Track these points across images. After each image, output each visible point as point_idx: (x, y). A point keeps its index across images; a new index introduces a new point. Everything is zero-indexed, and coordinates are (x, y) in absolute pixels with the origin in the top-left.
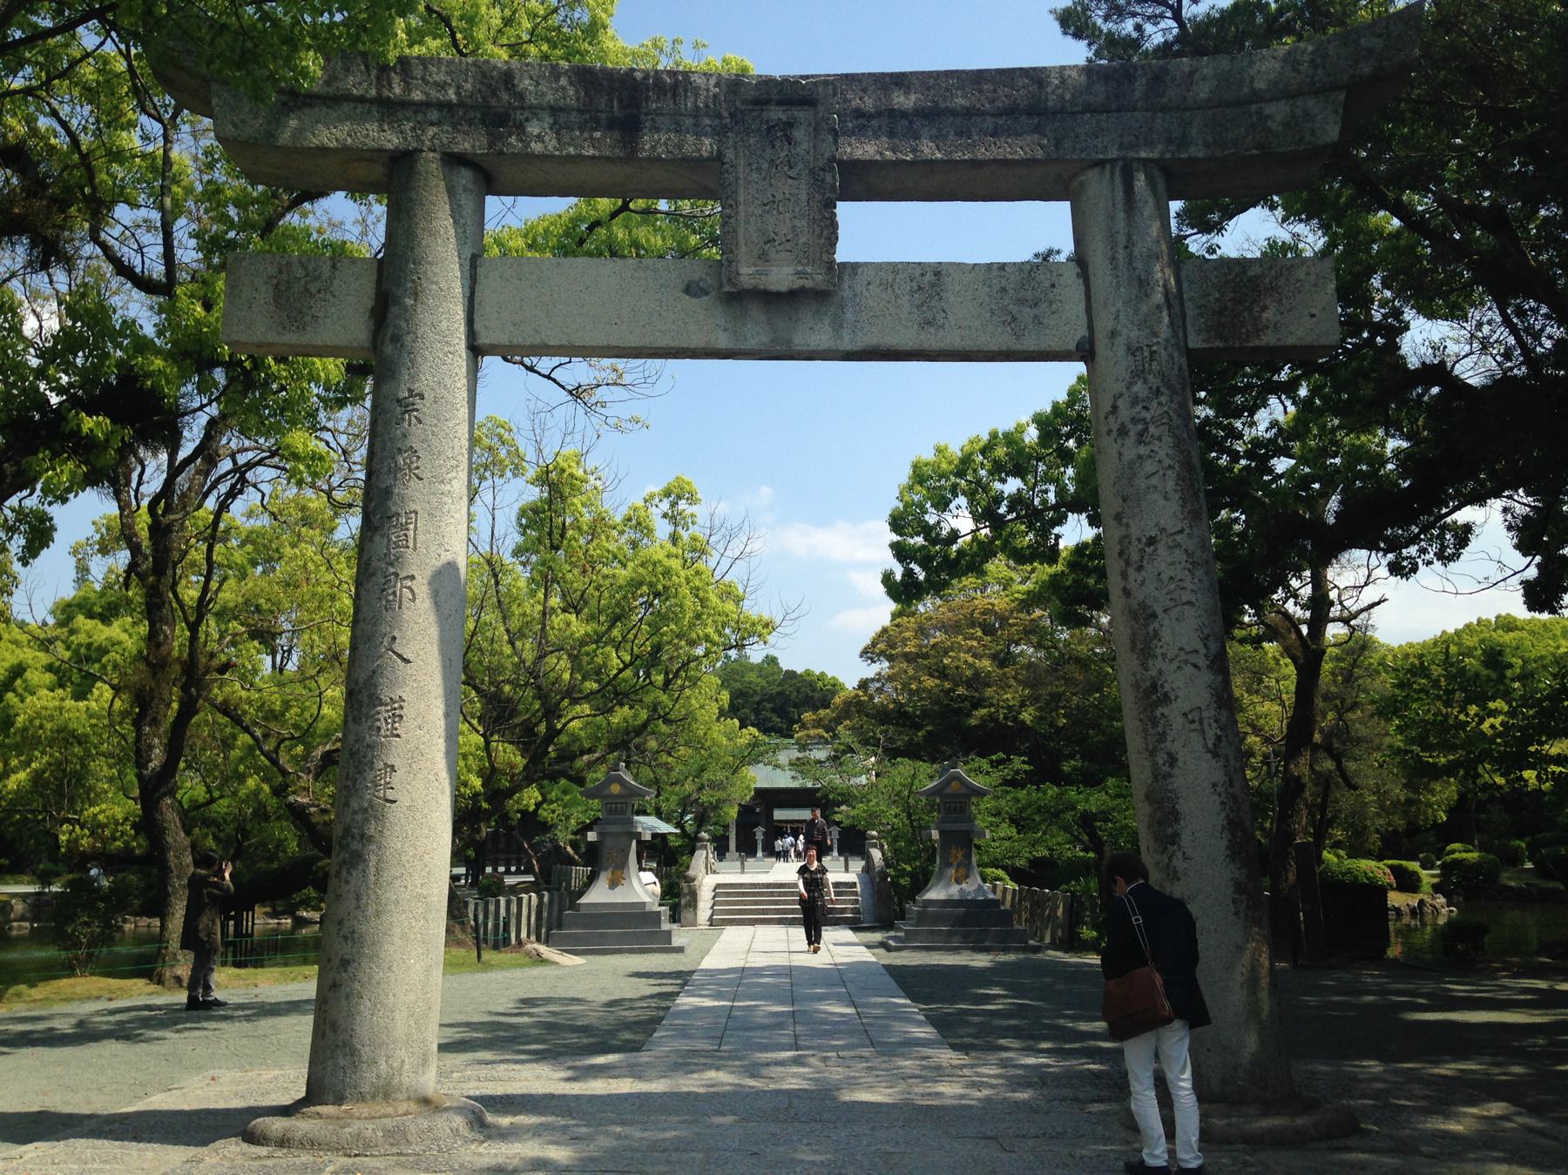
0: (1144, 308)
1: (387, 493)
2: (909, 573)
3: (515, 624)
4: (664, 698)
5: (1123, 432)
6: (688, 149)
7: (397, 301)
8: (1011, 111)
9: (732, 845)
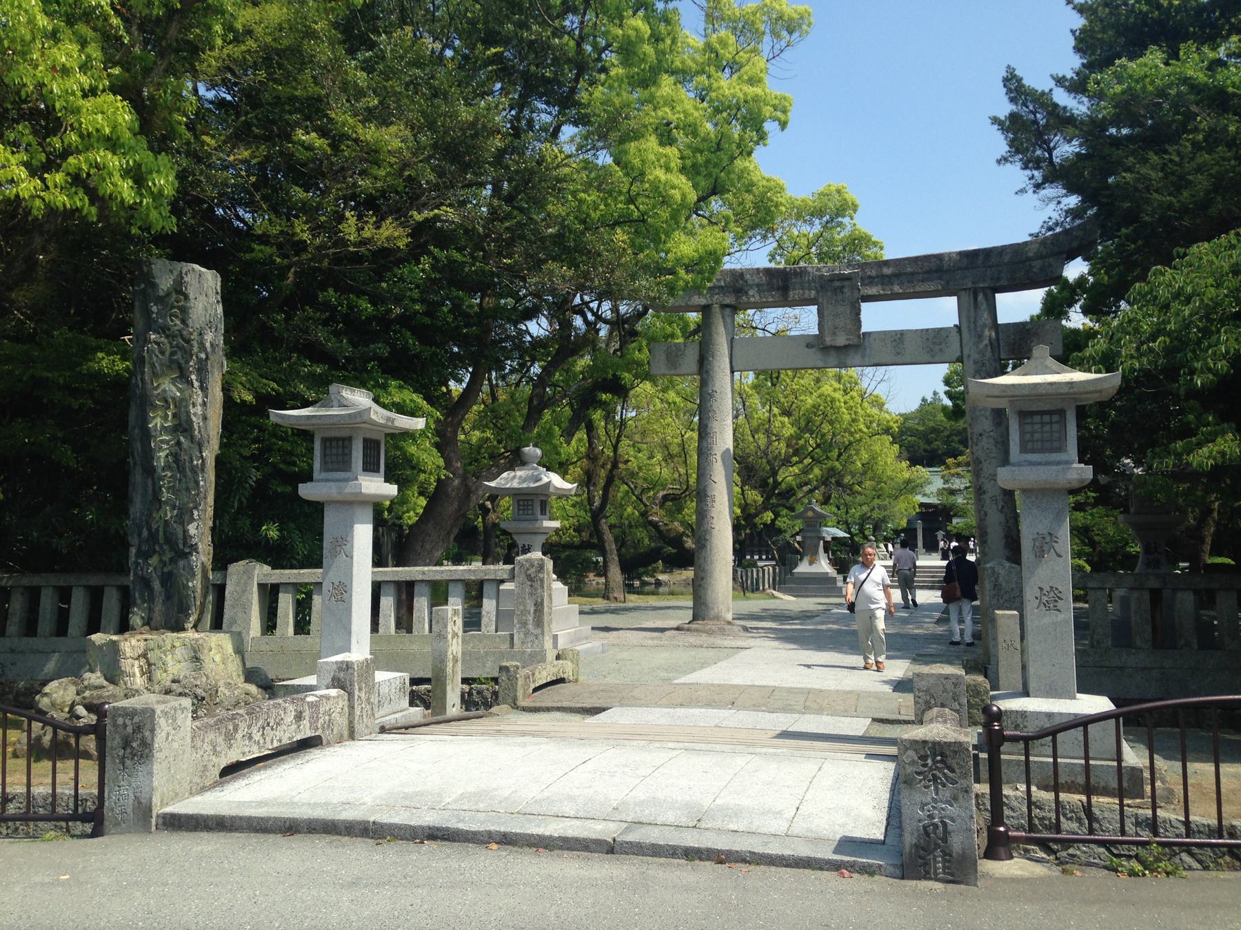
0: (981, 346)
1: (706, 426)
3: (755, 423)
4: (837, 464)
6: (806, 296)
8: (929, 272)
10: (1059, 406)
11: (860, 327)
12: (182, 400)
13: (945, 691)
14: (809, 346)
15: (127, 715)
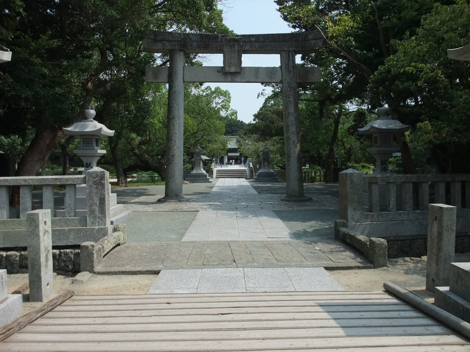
9: (218, 162)
14: (218, 72)
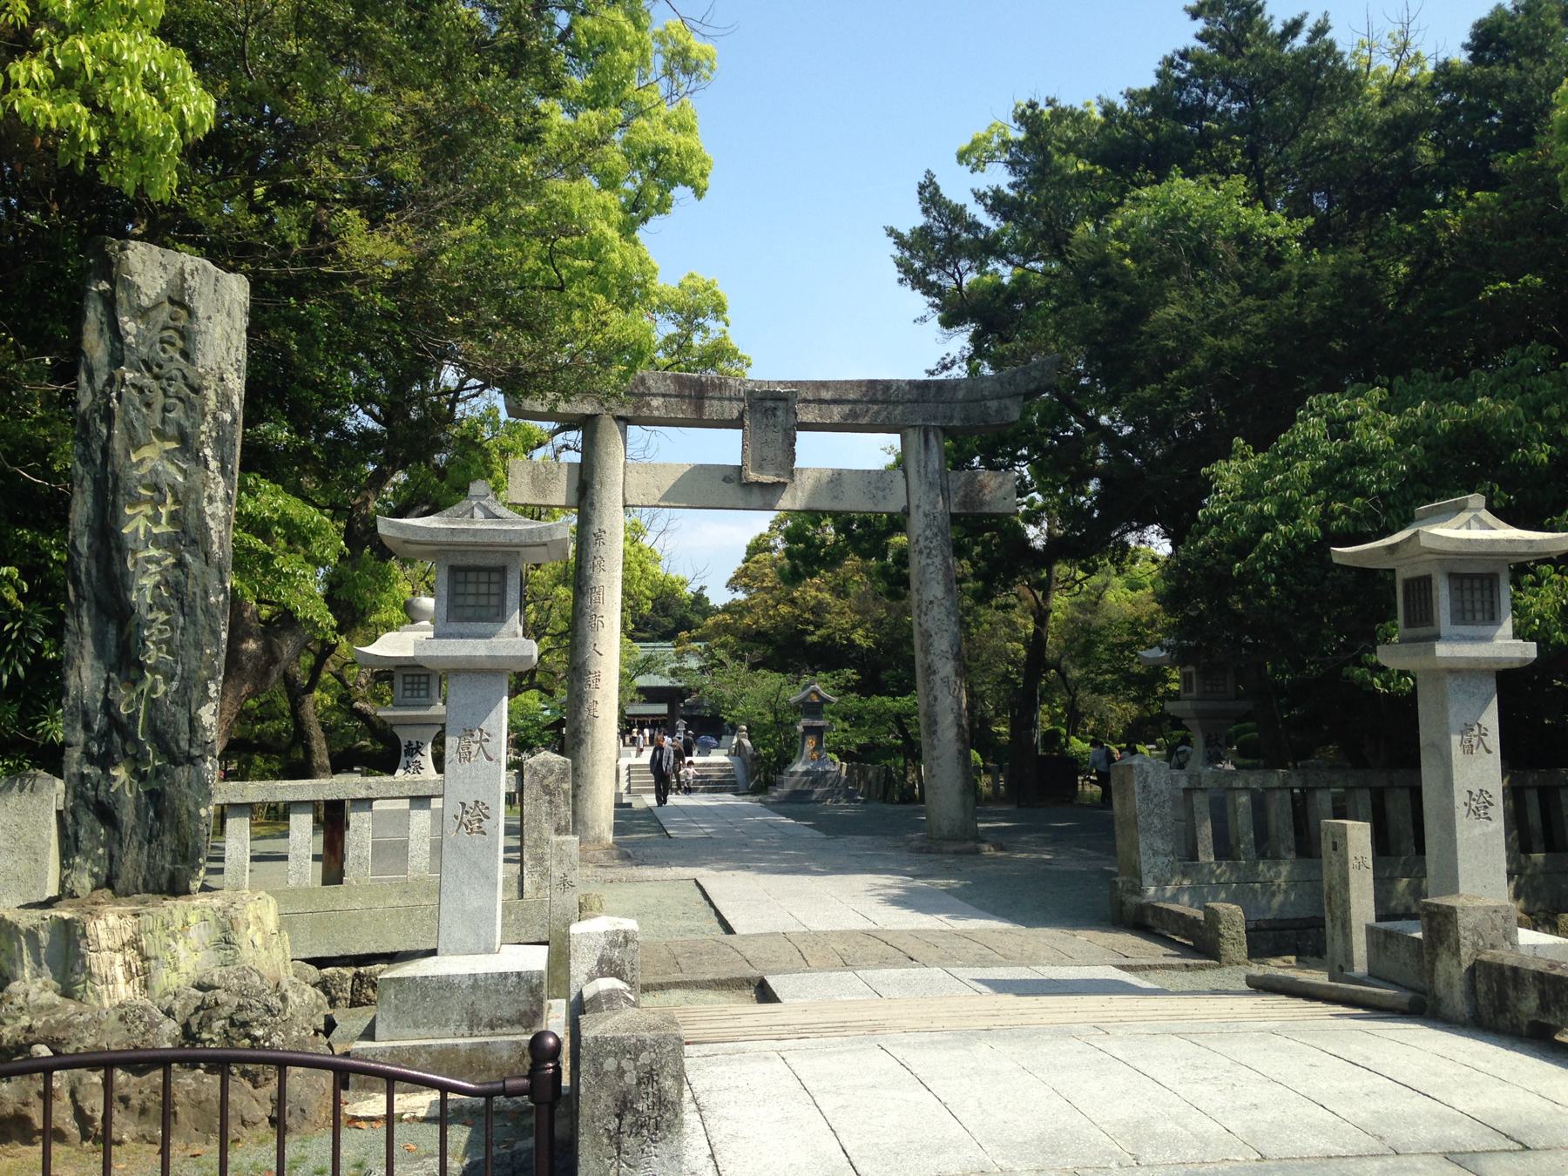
2: (794, 567)
5: (921, 552)
7: (592, 487)
10: (1491, 569)
11: (793, 460)
12: (188, 490)
13: (1494, 928)
14: (726, 479)
15: (625, 1051)
